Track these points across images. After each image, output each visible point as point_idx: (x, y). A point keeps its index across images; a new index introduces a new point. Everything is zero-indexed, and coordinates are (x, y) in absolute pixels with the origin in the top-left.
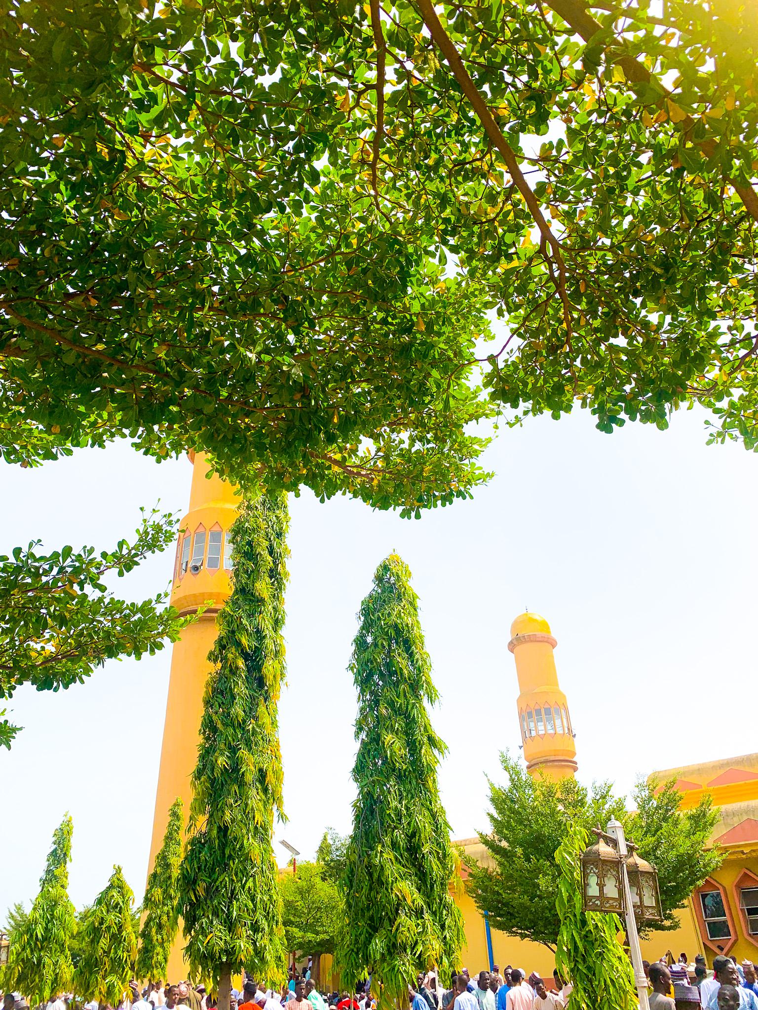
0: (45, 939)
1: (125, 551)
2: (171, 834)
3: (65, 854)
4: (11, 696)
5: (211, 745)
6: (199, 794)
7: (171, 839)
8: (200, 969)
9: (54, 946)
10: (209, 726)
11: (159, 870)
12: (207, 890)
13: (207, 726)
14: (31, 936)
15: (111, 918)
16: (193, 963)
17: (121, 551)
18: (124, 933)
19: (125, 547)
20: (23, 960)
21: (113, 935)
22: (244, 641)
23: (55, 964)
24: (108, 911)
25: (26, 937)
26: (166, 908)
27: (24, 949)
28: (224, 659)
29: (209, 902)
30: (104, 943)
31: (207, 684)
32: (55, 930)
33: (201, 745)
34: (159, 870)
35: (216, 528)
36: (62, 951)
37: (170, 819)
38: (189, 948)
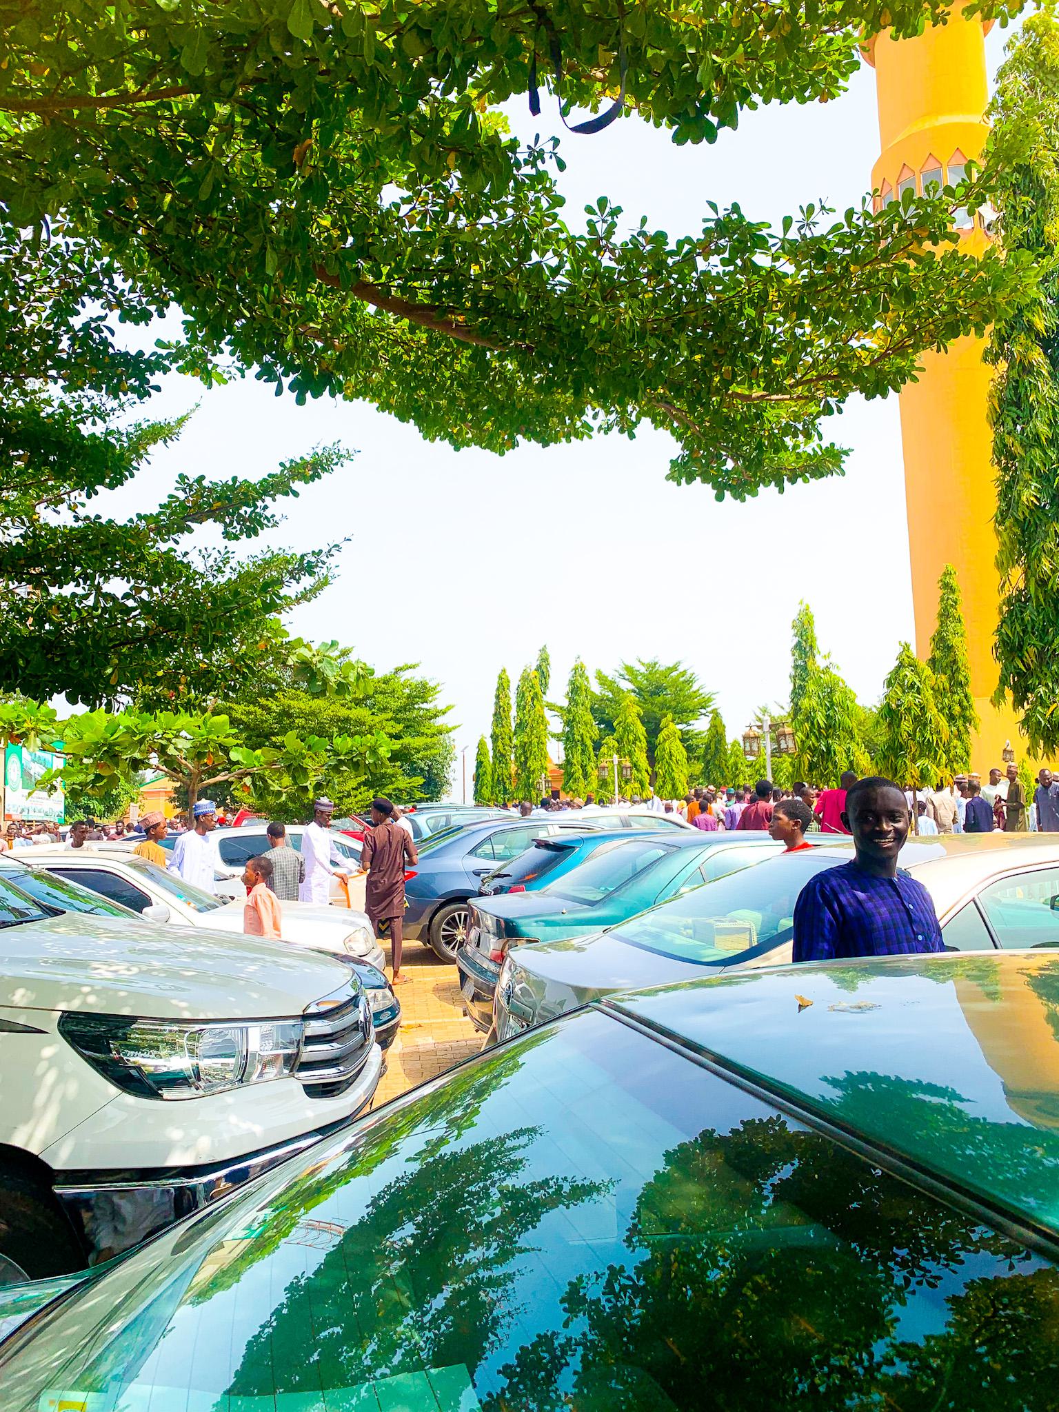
0: (828, 727)
1: (975, 176)
2: (945, 609)
3: (811, 646)
4: (840, 411)
5: (1012, 476)
6: (1004, 544)
7: (948, 617)
8: (1041, 742)
9: (842, 734)
10: (1003, 452)
11: (938, 654)
12: (1040, 655)
13: (1001, 453)
14: (813, 724)
15: (909, 699)
16: (1032, 737)
17: (970, 177)
18: (928, 715)
19: (974, 170)
20: (809, 748)
21: (915, 717)
22: (1040, 325)
23: (848, 751)
24: (904, 692)
25: (807, 725)
26: (956, 697)
27: (807, 737)
28: (1009, 357)
29: (1044, 669)
30: (906, 726)
31: (991, 396)
32: (838, 717)
33: (998, 480)
34: (938, 654)
35: (932, 165)
36: (852, 738)
37: (941, 592)
38: (1026, 722)
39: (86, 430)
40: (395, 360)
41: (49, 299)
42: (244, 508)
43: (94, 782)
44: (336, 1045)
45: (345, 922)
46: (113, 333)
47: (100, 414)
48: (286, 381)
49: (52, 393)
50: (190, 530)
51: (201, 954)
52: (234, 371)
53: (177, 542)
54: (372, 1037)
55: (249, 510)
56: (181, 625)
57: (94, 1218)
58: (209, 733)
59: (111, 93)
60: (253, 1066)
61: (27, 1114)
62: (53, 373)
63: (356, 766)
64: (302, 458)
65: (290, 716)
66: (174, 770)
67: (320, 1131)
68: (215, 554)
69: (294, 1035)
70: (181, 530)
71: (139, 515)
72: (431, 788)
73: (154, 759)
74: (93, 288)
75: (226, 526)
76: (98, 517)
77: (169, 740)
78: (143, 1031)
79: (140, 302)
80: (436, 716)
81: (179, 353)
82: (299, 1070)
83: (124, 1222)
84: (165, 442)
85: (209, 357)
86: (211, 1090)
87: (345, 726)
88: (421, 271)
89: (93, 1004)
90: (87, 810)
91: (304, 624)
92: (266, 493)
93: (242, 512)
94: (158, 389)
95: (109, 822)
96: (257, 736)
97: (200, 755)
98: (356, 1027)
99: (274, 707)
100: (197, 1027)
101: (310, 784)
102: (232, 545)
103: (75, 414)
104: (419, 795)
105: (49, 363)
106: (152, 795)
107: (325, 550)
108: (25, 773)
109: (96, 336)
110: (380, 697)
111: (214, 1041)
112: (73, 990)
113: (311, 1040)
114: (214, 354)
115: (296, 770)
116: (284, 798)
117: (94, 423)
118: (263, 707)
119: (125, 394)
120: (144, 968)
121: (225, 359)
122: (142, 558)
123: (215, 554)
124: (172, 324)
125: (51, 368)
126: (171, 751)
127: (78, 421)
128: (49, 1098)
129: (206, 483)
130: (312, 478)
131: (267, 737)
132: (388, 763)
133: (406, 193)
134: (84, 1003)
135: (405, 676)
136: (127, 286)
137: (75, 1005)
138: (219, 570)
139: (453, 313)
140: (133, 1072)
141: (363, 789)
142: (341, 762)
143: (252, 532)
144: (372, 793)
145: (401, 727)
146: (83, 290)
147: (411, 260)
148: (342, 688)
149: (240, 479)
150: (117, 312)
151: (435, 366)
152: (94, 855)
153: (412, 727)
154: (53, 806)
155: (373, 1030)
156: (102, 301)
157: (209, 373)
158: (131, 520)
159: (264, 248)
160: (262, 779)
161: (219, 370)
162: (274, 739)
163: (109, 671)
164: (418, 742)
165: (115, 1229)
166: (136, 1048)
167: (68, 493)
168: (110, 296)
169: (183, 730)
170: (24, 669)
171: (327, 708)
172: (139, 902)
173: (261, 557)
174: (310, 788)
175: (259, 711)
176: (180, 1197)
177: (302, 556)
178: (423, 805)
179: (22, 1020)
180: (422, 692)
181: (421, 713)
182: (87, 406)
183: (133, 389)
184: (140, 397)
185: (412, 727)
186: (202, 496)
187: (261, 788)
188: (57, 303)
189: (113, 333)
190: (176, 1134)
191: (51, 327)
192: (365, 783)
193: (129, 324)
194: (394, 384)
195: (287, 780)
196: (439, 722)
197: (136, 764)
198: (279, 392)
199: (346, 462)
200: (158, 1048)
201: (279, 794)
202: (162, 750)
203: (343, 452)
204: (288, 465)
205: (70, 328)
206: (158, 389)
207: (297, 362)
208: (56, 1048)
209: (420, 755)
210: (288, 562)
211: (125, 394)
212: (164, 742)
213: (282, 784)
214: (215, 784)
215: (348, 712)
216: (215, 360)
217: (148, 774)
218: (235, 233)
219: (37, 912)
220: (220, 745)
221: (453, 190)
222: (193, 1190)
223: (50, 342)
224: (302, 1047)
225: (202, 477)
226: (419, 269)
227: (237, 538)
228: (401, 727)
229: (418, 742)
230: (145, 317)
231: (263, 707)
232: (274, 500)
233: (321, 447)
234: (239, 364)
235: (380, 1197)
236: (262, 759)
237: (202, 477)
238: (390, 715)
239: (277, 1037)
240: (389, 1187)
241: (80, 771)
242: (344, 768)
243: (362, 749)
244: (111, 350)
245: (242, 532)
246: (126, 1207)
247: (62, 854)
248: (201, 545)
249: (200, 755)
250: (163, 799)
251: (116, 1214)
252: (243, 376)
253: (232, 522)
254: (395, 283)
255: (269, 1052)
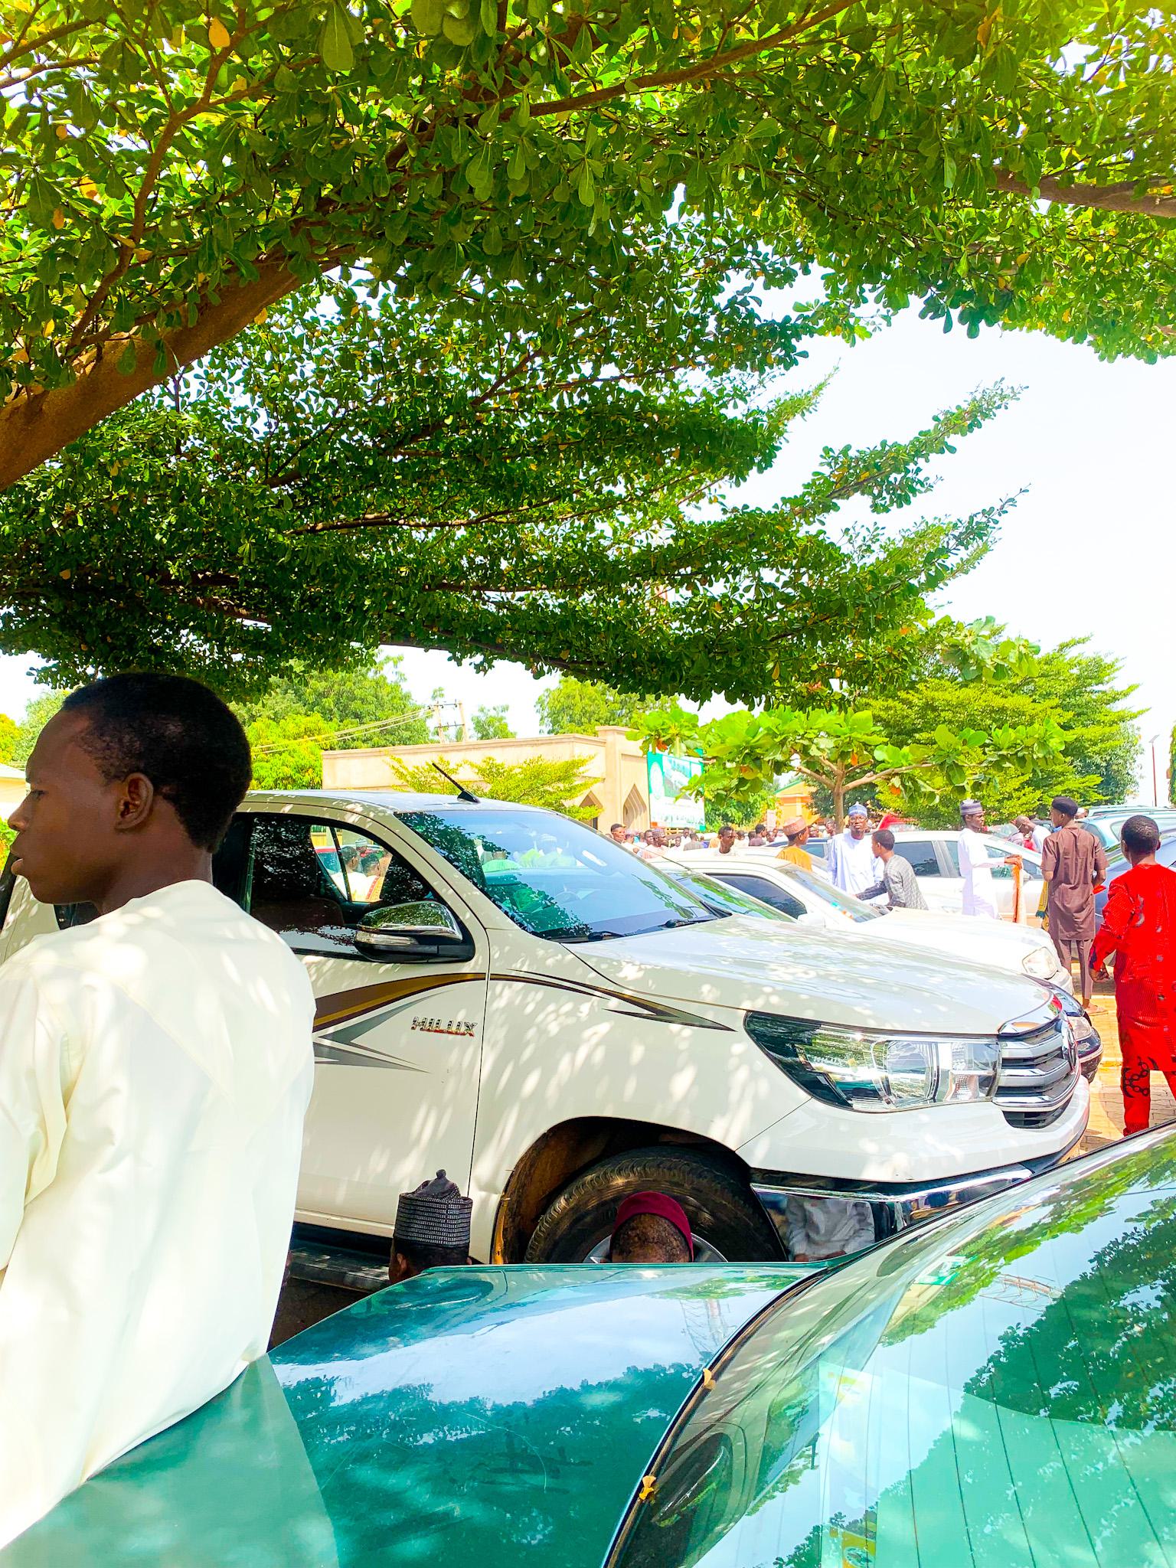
39: (730, 413)
40: (1075, 264)
41: (694, 281)
42: (894, 475)
43: (737, 787)
44: (1037, 1071)
45: (1023, 940)
46: (759, 302)
47: (741, 395)
48: (955, 313)
49: (694, 381)
50: (836, 508)
51: (881, 964)
52: (879, 320)
53: (823, 524)
54: (1078, 1067)
55: (899, 477)
56: (842, 610)
57: (787, 1222)
58: (852, 730)
59: (775, 29)
60: (945, 1082)
61: (722, 1108)
62: (701, 359)
63: (1022, 760)
64: (958, 407)
65: (934, 709)
66: (817, 772)
67: (1026, 1164)
68: (864, 533)
69: (989, 1056)
70: (827, 508)
71: (783, 499)
72: (1111, 787)
73: (796, 761)
74: (736, 259)
75: (875, 498)
76: (746, 507)
77: (810, 739)
78: (824, 1037)
79: (783, 263)
80: (1115, 699)
81: (824, 311)
82: (998, 1094)
83: (817, 1230)
84: (803, 414)
85: (852, 310)
86: (903, 1107)
87: (999, 716)
88: (1115, 140)
89: (775, 1005)
90: (726, 817)
91: (952, 604)
92: (918, 453)
93: (891, 479)
94: (805, 354)
95: (747, 828)
96: (900, 733)
97: (843, 755)
98: (1060, 1054)
99: (916, 701)
100: (883, 1038)
101: (967, 783)
102: (882, 518)
103: (718, 399)
104: (1095, 797)
105: (697, 349)
106: (788, 798)
107: (997, 506)
108: (667, 782)
109: (742, 309)
110: (1041, 681)
111: (902, 1054)
112: (756, 991)
113: (1008, 1063)
114: (858, 306)
115: (950, 768)
116: (937, 800)
117: (735, 406)
118: (903, 701)
119: (771, 367)
120: (822, 973)
121: (869, 310)
122: (792, 545)
123: (864, 533)
124: (810, 287)
125: (699, 353)
126: (813, 751)
127: (721, 407)
128: (742, 1095)
129: (852, 453)
130: (970, 428)
131: (910, 733)
132: (1061, 756)
133: (1091, 49)
134: (767, 1003)
135: (1072, 653)
136: (769, 249)
137: (758, 1006)
138: (869, 549)
139: (1157, 185)
140: (821, 1078)
141: (1027, 789)
142: (1003, 758)
143: (902, 500)
144: (1038, 794)
145: (1070, 714)
146: (728, 264)
147: (1102, 131)
148: (1000, 671)
149: (890, 443)
150: (762, 279)
151: (1130, 260)
152: (746, 858)
153: (1084, 714)
154: (693, 813)
155: (1079, 1061)
156: (746, 270)
157: (852, 328)
158: (776, 506)
159: (941, 161)
160: (912, 779)
161: (862, 323)
162: (917, 736)
163: (770, 666)
164: (1092, 732)
165: (808, 1236)
166: (820, 1054)
167: (708, 487)
168: (754, 263)
169: (823, 730)
170: (689, 669)
171: (979, 698)
172: (793, 909)
173: (913, 530)
174: (968, 788)
175: (899, 706)
176: (887, 1216)
177: (971, 518)
178: (1103, 808)
179: (710, 1015)
180: (1096, 671)
181: (1094, 696)
182: (729, 387)
183: (780, 360)
184: (787, 368)
185: (1084, 714)
186: (849, 467)
187: (912, 790)
188: (703, 284)
189: (759, 302)
190: (870, 1147)
191: (698, 311)
192: (1028, 783)
193: (774, 290)
194: (1071, 295)
195: (940, 780)
196: (1117, 707)
197: (779, 767)
198: (948, 328)
199: (1011, 403)
200: (842, 1056)
201: (932, 795)
202: (805, 751)
203: (1007, 392)
204: (942, 417)
205: (716, 308)
206: (805, 354)
207: (968, 288)
208: (744, 1045)
209: (1096, 748)
210: (955, 526)
211: (771, 367)
212: (806, 742)
213: (935, 785)
214: (855, 788)
215: (1003, 701)
216: (857, 312)
217: (784, 779)
218: (905, 150)
219: (703, 913)
220: (865, 744)
221: (1155, 26)
222: (891, 1207)
223: (698, 327)
224: (999, 1070)
225: (848, 448)
226: (1112, 140)
227: (887, 510)
228: (1070, 714)
229: (1092, 732)
230: (789, 277)
231: (903, 701)
232: (927, 461)
233: (980, 390)
234: (884, 312)
235: (1104, 1253)
236: (911, 757)
237: (848, 448)
238: (1057, 701)
239: (968, 1055)
240: (1116, 1243)
241: (724, 776)
242: (1008, 765)
243: (1029, 742)
244: (757, 322)
245: (892, 502)
246: (818, 1216)
247: (707, 860)
248: (852, 525)
249: (843, 755)
250: (799, 808)
251: (807, 1221)
252: (889, 324)
253: (880, 494)
254: (1078, 167)
255: (961, 1070)
